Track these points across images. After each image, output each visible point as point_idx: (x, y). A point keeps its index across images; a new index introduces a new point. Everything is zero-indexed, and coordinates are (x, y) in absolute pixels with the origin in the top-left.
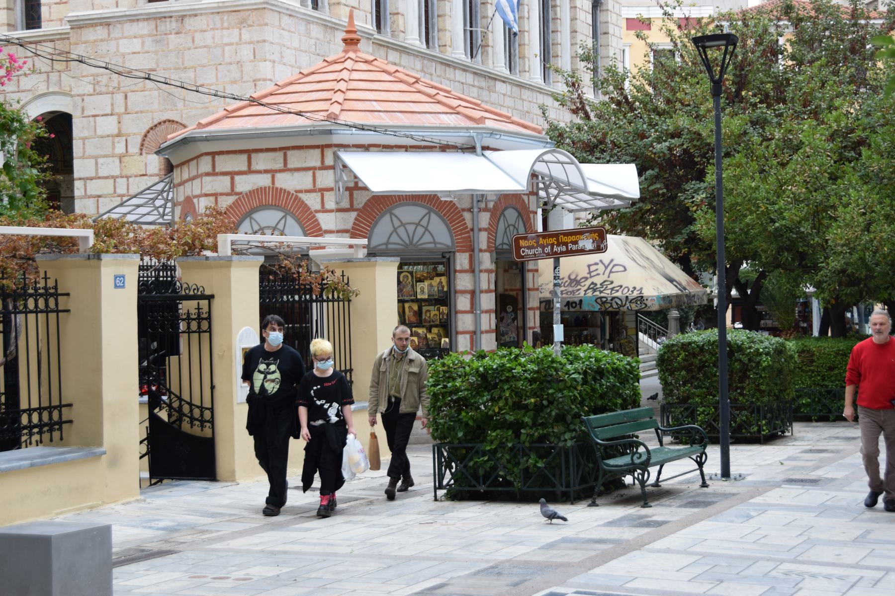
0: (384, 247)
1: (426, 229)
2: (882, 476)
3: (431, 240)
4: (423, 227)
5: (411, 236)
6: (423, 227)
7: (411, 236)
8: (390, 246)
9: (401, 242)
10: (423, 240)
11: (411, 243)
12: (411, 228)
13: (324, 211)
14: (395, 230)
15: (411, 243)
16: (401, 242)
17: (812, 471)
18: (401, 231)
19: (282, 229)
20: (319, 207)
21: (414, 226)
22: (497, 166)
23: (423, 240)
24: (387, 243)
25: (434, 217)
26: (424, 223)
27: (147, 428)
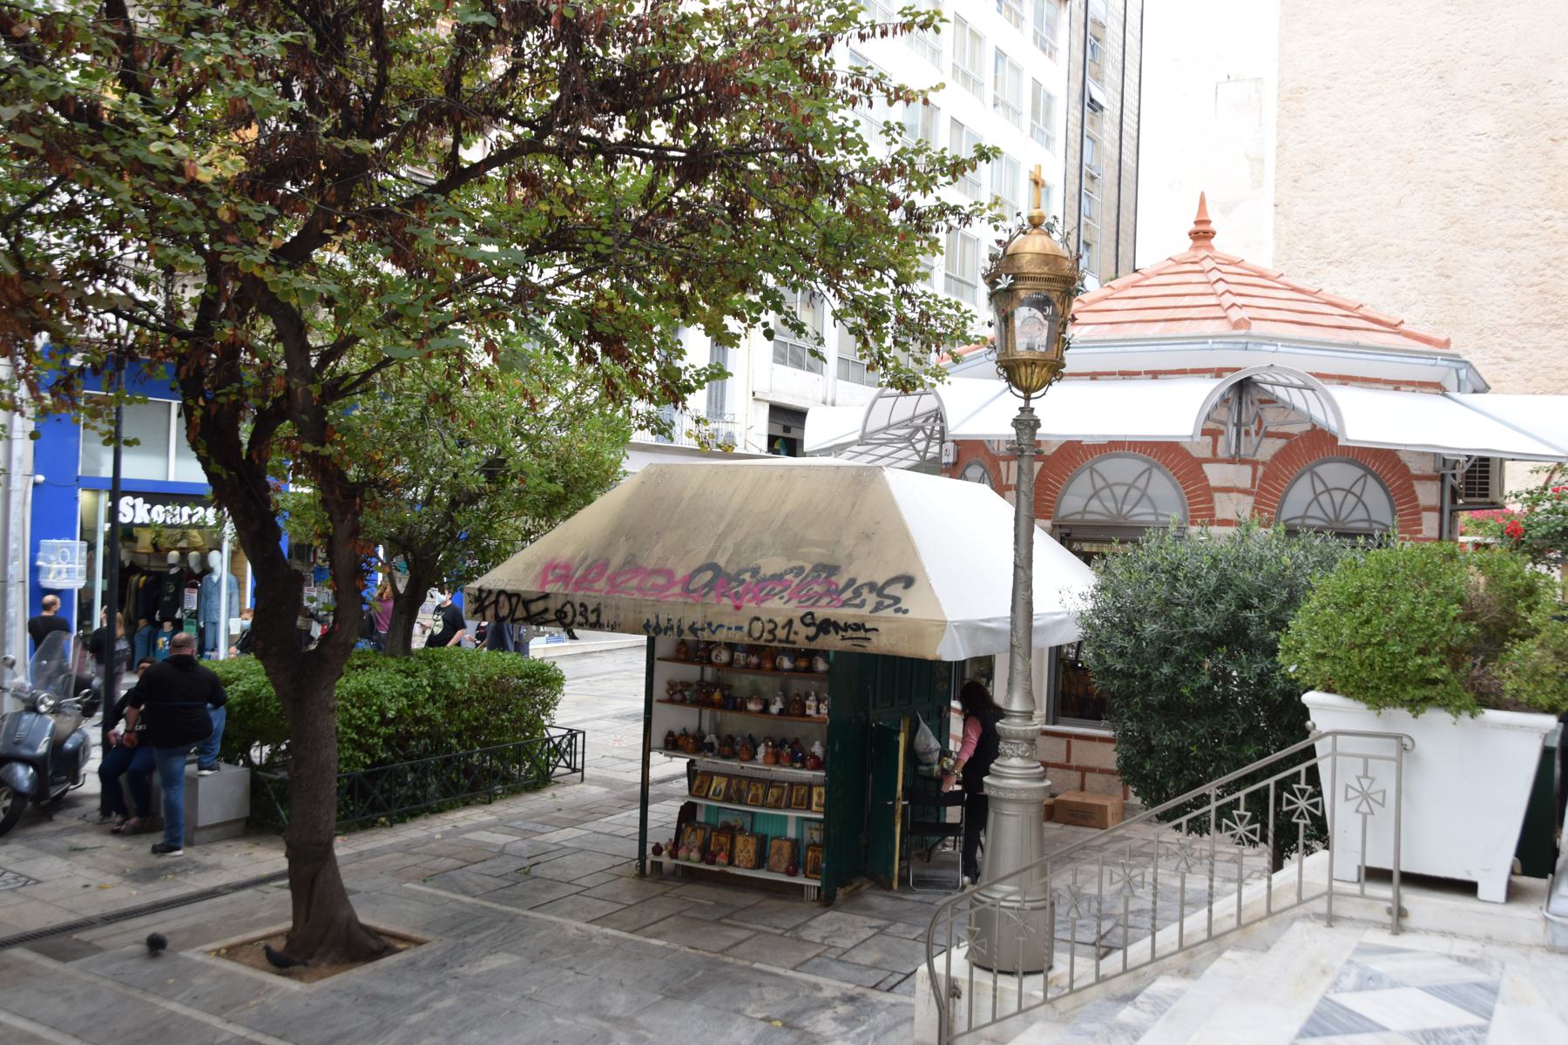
0: (1078, 517)
1: (1359, 499)
2: (467, 836)
3: (1366, 517)
4: (1103, 488)
5: (1338, 507)
6: (1103, 488)
7: (1338, 507)
8: (1088, 517)
9: (1321, 515)
10: (1354, 516)
11: (1337, 518)
12: (1338, 496)
13: (1214, 459)
14: (1316, 497)
15: (1337, 518)
16: (1321, 515)
17: (650, 937)
18: (1324, 499)
19: (1103, 484)
20: (1208, 454)
21: (1343, 493)
22: (968, 418)
23: (1354, 516)
24: (1085, 511)
25: (1320, 470)
26: (1357, 490)
27: (1547, 753)
